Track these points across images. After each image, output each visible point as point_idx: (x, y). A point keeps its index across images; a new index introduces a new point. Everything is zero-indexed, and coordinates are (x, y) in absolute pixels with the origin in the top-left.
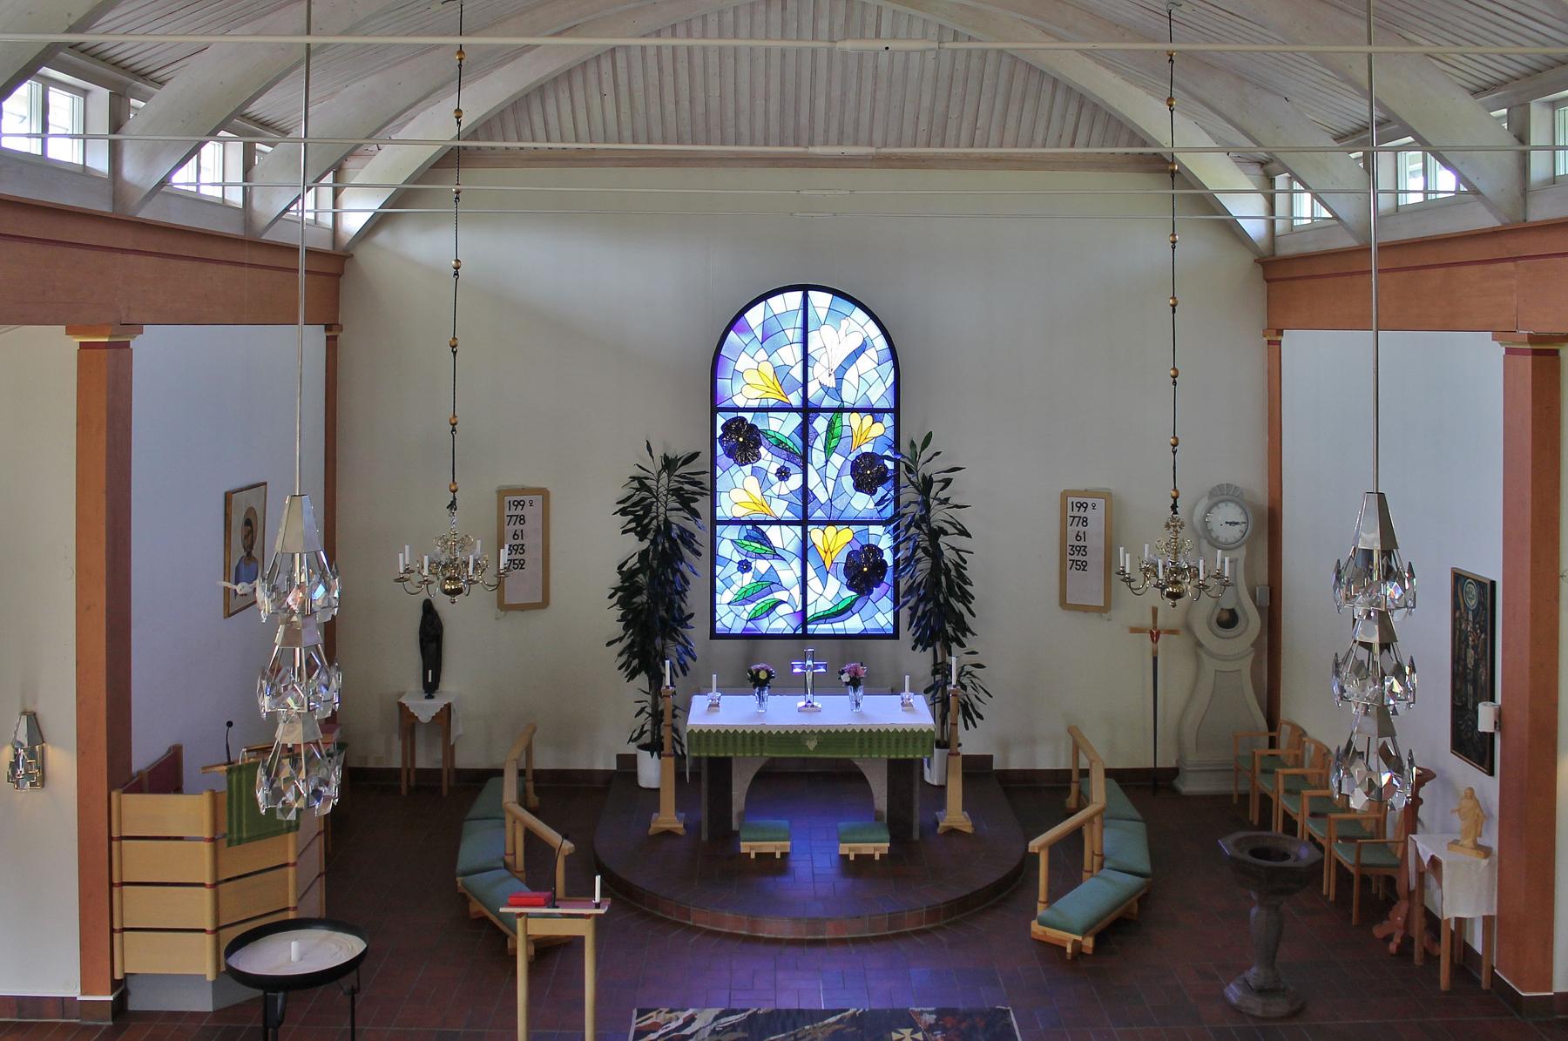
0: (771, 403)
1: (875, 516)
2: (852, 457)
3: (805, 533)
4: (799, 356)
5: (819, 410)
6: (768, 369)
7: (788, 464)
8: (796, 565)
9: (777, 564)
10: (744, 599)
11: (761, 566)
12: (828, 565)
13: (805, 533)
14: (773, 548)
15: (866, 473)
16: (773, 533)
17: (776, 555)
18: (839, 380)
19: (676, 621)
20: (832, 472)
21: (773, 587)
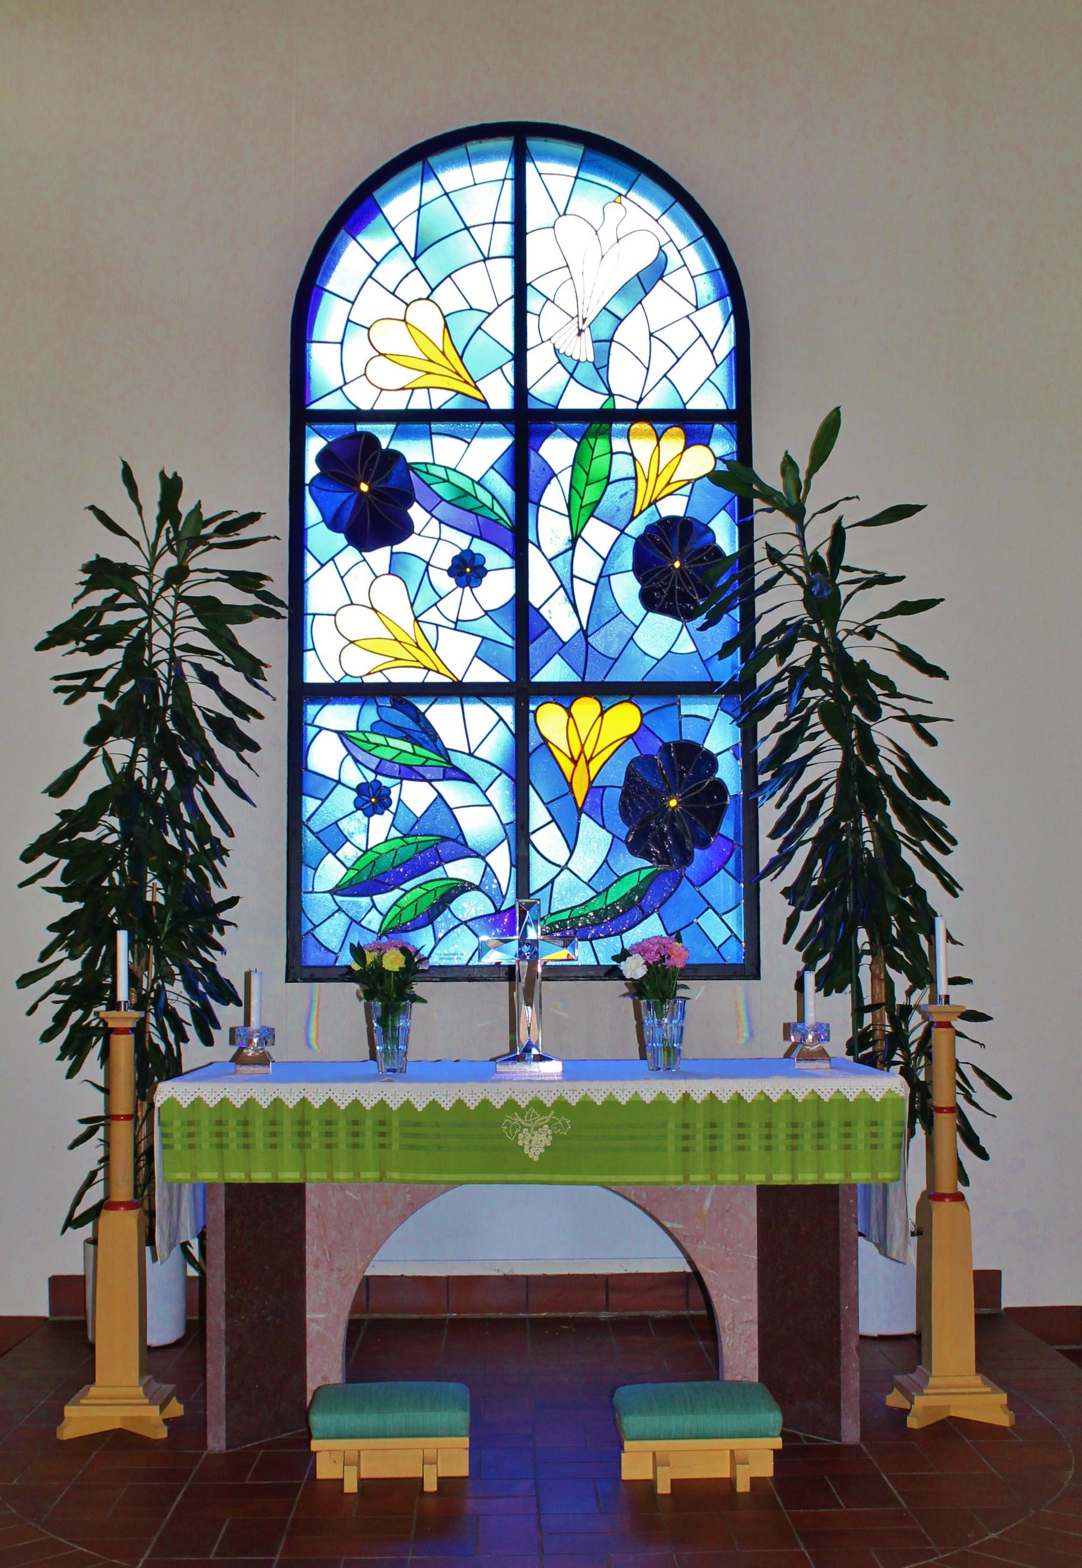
0: (439, 400)
1: (696, 673)
2: (636, 529)
3: (523, 720)
4: (507, 288)
5: (555, 418)
6: (427, 318)
7: (480, 547)
8: (501, 792)
9: (453, 792)
10: (367, 882)
11: (416, 796)
12: (580, 790)
13: (523, 720)
14: (444, 752)
15: (674, 566)
16: (443, 717)
17: (455, 774)
18: (605, 344)
19: (192, 921)
20: (587, 565)
21: (445, 849)
